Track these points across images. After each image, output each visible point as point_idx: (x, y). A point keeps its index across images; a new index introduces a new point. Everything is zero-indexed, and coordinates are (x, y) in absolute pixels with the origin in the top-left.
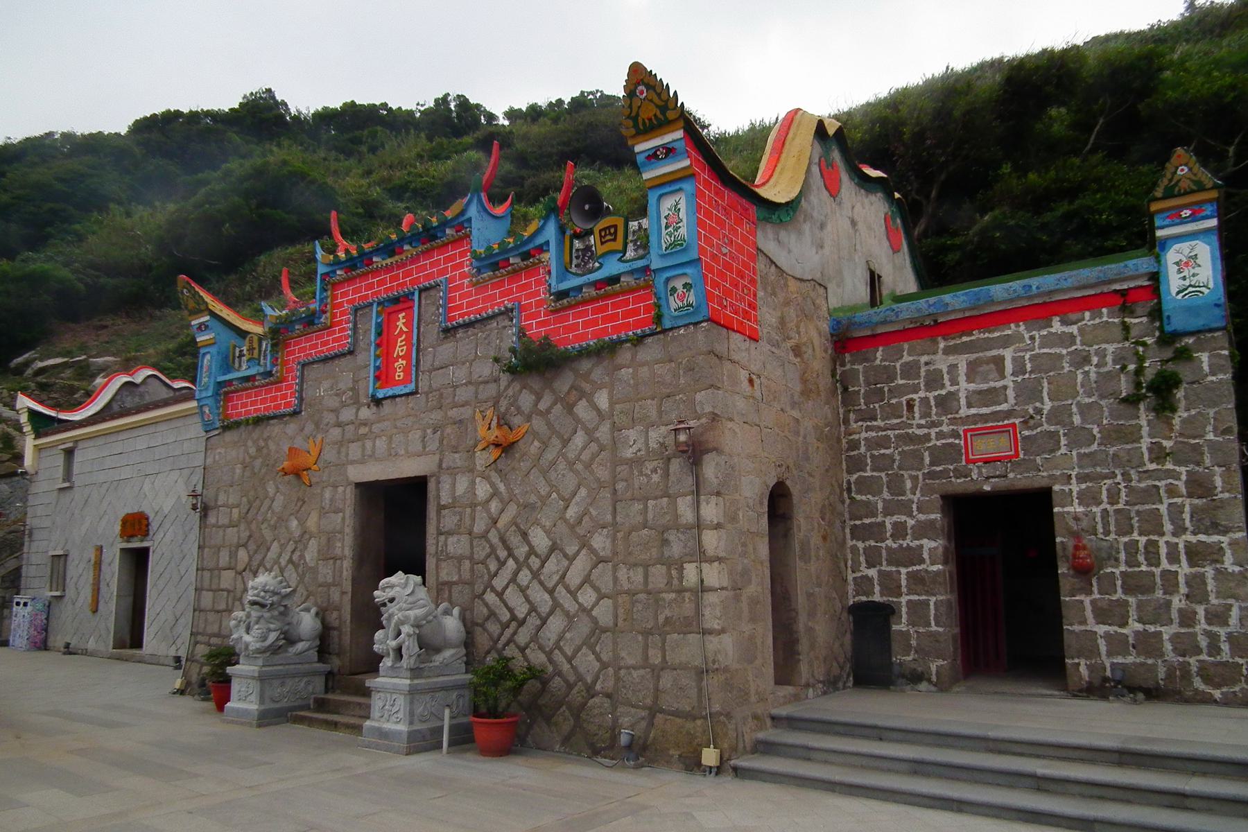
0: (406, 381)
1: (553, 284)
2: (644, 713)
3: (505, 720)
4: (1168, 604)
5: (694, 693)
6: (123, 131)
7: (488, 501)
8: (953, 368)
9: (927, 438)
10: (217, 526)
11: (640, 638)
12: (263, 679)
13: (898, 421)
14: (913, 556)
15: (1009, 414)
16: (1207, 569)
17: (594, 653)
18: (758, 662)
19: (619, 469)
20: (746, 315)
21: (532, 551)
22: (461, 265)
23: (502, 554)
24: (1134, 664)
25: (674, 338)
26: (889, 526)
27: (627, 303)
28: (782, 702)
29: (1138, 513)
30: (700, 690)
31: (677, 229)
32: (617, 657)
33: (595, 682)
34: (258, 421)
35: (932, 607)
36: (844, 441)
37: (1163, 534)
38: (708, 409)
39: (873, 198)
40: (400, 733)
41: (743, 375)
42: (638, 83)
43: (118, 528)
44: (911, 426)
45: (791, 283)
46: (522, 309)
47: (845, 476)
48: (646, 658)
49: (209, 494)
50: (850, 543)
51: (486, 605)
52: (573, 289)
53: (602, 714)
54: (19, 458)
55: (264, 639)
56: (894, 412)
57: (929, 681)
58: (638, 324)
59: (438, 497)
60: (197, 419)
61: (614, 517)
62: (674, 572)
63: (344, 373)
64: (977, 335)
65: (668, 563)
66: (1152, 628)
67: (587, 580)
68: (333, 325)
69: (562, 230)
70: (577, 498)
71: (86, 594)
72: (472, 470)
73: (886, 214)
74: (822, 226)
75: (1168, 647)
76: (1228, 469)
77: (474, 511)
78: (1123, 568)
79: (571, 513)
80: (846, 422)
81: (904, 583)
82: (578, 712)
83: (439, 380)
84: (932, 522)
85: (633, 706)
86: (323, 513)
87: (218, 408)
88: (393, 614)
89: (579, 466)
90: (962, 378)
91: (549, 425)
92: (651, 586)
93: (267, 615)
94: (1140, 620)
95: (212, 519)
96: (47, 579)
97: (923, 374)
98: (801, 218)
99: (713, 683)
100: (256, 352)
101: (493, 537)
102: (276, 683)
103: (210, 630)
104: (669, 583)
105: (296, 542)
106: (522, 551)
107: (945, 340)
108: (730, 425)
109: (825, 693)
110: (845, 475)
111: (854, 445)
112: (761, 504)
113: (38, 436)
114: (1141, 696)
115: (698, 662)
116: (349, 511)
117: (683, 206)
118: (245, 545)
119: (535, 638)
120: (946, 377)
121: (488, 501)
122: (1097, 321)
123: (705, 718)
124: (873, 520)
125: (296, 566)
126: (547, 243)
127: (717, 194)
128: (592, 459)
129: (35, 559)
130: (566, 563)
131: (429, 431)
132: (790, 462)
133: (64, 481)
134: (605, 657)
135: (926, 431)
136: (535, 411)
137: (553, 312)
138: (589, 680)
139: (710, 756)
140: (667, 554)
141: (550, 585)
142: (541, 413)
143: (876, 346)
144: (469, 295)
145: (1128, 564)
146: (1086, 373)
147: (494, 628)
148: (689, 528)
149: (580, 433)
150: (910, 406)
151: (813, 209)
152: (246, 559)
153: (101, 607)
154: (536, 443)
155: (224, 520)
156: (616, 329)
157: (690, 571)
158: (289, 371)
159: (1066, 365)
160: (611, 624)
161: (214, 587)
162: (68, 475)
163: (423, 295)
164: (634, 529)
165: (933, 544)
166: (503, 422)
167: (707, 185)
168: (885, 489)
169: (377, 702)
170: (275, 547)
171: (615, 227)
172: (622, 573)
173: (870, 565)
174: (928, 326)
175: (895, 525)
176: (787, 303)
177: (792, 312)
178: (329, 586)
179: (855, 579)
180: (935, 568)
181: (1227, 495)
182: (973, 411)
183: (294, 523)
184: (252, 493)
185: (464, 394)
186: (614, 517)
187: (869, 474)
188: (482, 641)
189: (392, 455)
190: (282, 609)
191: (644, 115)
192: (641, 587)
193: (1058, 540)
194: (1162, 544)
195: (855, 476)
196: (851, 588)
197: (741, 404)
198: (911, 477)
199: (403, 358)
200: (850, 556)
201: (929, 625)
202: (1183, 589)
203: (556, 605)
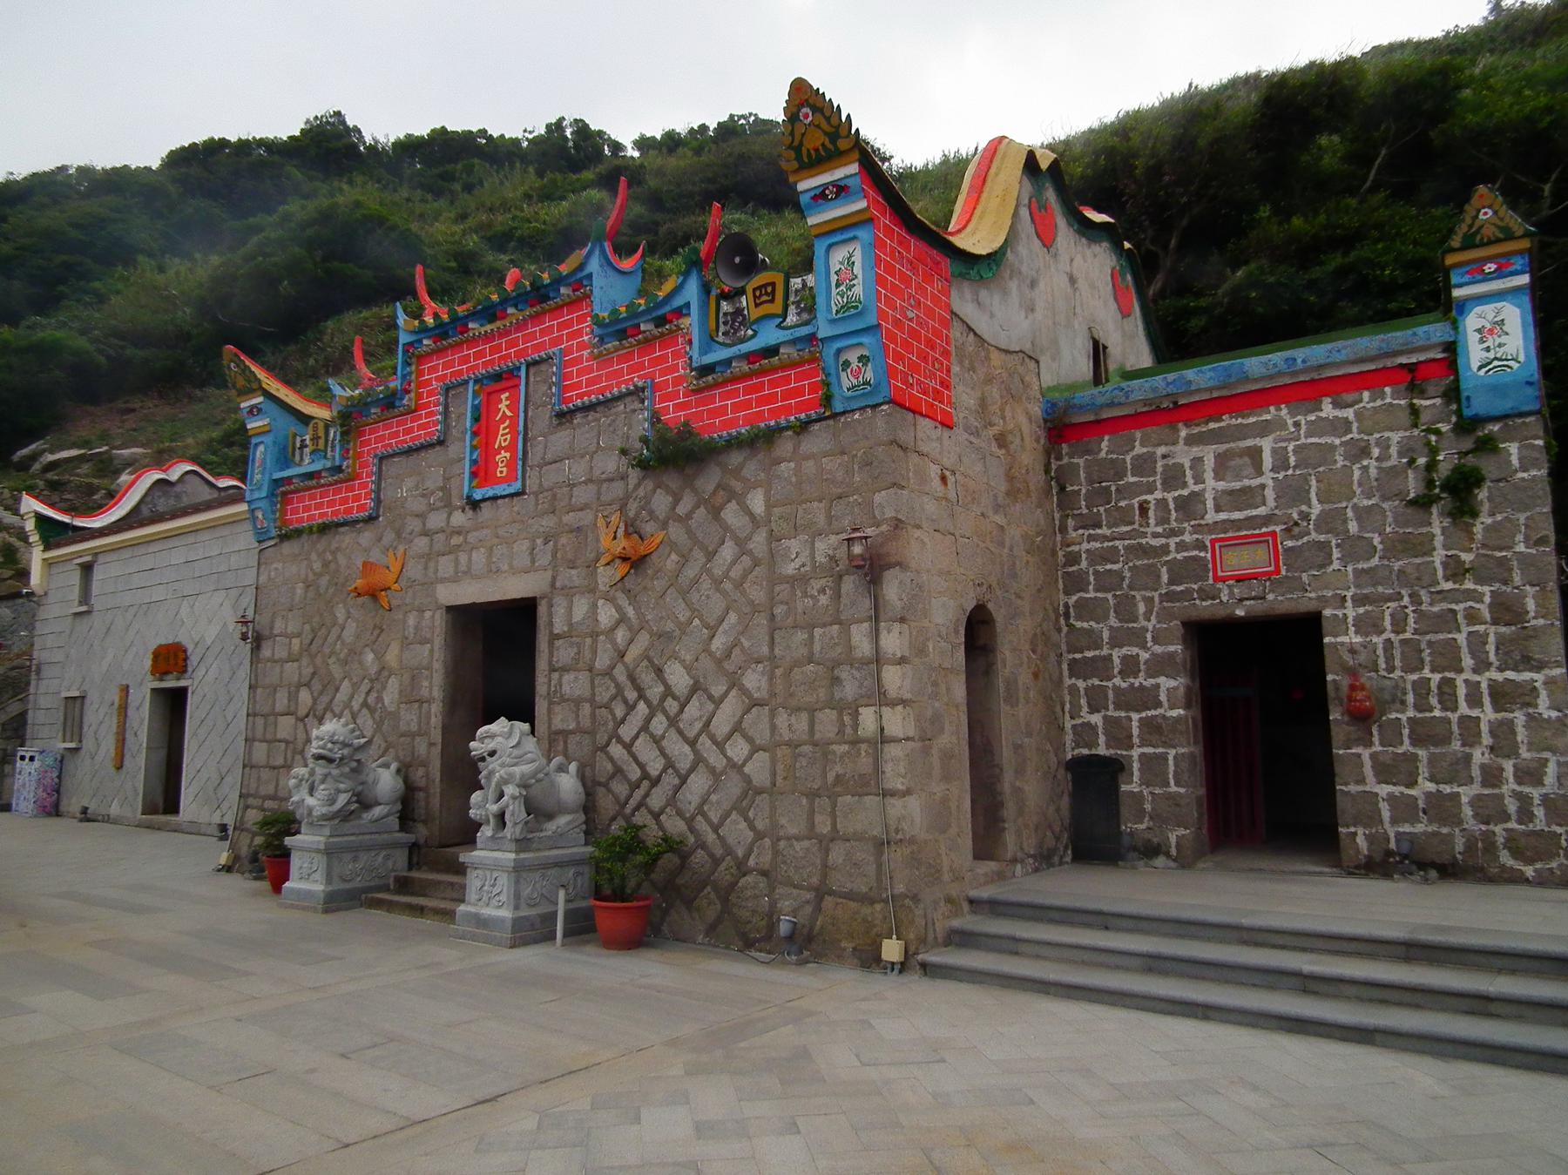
0: (509, 479)
1: (695, 356)
2: (809, 896)
3: (635, 903)
4: (1468, 759)
5: (871, 869)
6: (155, 164)
7: (613, 629)
8: (1197, 462)
9: (1165, 549)
12: (330, 852)
13: (1128, 528)
14: (1147, 699)
15: (1268, 519)
17: (746, 819)
18: (953, 830)
19: (777, 589)
20: (938, 395)
21: (668, 692)
22: (579, 333)
23: (631, 695)
24: (1425, 833)
26: (1117, 661)
27: (787, 380)
28: (982, 881)
29: (1430, 644)
30: (879, 866)
31: (850, 288)
32: (775, 826)
33: (747, 856)
34: (325, 529)
36: (1061, 553)
37: (1460, 671)
38: (889, 513)
39: (1097, 248)
41: (934, 471)
43: (148, 663)
44: (1144, 535)
45: (994, 355)
46: (656, 387)
48: (812, 825)
49: (263, 620)
51: (611, 759)
53: (756, 897)
54: (24, 574)
55: (332, 801)
56: (1124, 517)
57: (1168, 855)
58: (801, 407)
59: (551, 624)
60: (248, 526)
61: (772, 648)
62: (846, 719)
63: (432, 469)
64: (1227, 421)
66: (1447, 789)
67: (737, 728)
69: (706, 288)
70: (725, 625)
71: (108, 746)
73: (1113, 269)
74: (1033, 284)
75: (1468, 812)
76: (1543, 589)
78: (1411, 713)
79: (718, 644)
80: (1063, 529)
81: (1135, 731)
82: (727, 894)
83: (551, 476)
84: (1171, 655)
86: (406, 643)
87: (274, 512)
88: (494, 770)
90: (1209, 475)
92: (817, 736)
93: (335, 772)
94: (1432, 779)
95: (266, 652)
96: (59, 726)
97: (1159, 469)
99: (895, 857)
100: (322, 442)
101: (620, 674)
102: (347, 857)
103: (263, 792)
104: (841, 732)
105: (371, 681)
106: (655, 691)
107: (1187, 426)
109: (1036, 870)
110: (1062, 596)
111: (1073, 559)
113: (47, 548)
114: (1433, 874)
115: (876, 831)
116: (438, 642)
117: (858, 258)
119: (672, 801)
120: (1189, 473)
121: (613, 629)
122: (1379, 403)
123: (886, 901)
124: (1097, 653)
125: (372, 711)
126: (688, 305)
127: (900, 243)
128: (744, 577)
129: (44, 702)
130: (711, 707)
131: (539, 541)
132: (993, 580)
133: (81, 603)
134: (760, 825)
135: (1163, 541)
136: (672, 515)
138: (740, 853)
139: (892, 950)
140: (837, 696)
141: (691, 734)
142: (679, 519)
143: (1101, 434)
144: (589, 370)
145: (1417, 707)
147: (620, 788)
148: (865, 662)
150: (1143, 509)
151: (1021, 262)
152: (309, 702)
153: (127, 762)
154: (674, 557)
155: (281, 653)
157: (868, 717)
158: (364, 465)
160: (768, 783)
161: (269, 737)
162: (85, 597)
163: (532, 371)
164: (798, 663)
165: (1172, 683)
166: (632, 529)
167: (889, 232)
168: (1112, 613)
169: (473, 881)
170: (346, 687)
171: (773, 284)
172: (782, 719)
173: (1093, 709)
175: (1124, 658)
176: (989, 380)
177: (994, 392)
178: (413, 735)
179: (1074, 727)
180: (1175, 713)
181: (1541, 622)
182: (1223, 516)
183: (370, 657)
185: (583, 495)
186: (772, 648)
187: (1092, 595)
188: (606, 804)
189: (492, 571)
190: (354, 764)
192: (805, 737)
193: (1330, 677)
194: (1460, 682)
195: (1075, 598)
196: (1069, 738)
199: (506, 449)
200: (1067, 698)
202: (1487, 740)
203: (699, 760)
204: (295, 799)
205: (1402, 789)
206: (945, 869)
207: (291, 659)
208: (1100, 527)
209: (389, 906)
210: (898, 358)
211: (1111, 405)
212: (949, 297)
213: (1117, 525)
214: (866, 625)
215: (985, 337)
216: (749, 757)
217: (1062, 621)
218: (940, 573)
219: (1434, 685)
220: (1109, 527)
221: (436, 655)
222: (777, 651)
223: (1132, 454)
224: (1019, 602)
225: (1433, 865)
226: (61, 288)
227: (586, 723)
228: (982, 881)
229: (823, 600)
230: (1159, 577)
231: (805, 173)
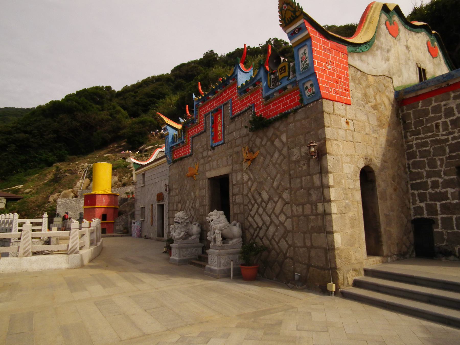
0: (221, 140)
1: (264, 94)
2: (305, 267)
3: (253, 267)
6: (169, 72)
9: (447, 140)
10: (173, 196)
11: (302, 235)
12: (179, 248)
13: (430, 134)
14: (443, 196)
17: (286, 241)
18: (357, 246)
20: (343, 94)
21: (263, 200)
23: (253, 202)
26: (429, 183)
27: (290, 97)
28: (374, 263)
30: (326, 258)
31: (305, 62)
34: (182, 159)
35: (454, 220)
36: (405, 145)
39: (419, 35)
41: (343, 120)
42: (283, 4)
43: (156, 198)
44: (438, 135)
45: (371, 79)
46: (255, 106)
47: (407, 161)
48: (305, 243)
50: (411, 191)
51: (249, 221)
55: (180, 234)
56: (430, 129)
57: (455, 255)
58: (295, 105)
59: (232, 181)
62: (314, 207)
67: (282, 211)
68: (200, 122)
70: (277, 179)
72: (242, 170)
74: (388, 51)
77: (243, 186)
79: (275, 184)
80: (406, 137)
81: (439, 209)
85: (301, 263)
86: (200, 189)
89: (277, 166)
91: (266, 150)
92: (305, 213)
93: (180, 226)
95: (171, 194)
101: (250, 195)
102: (184, 250)
104: (312, 212)
106: (259, 200)
107: (454, 92)
108: (335, 142)
109: (398, 260)
110: (407, 161)
112: (356, 176)
116: (207, 188)
117: (307, 52)
118: (180, 202)
119: (265, 235)
123: (328, 270)
124: (422, 180)
125: (194, 209)
126: (261, 78)
127: (324, 43)
130: (274, 205)
131: (228, 157)
134: (290, 242)
135: (446, 137)
137: (266, 105)
138: (284, 252)
141: (269, 214)
142: (263, 146)
143: (419, 100)
147: (252, 231)
148: (318, 188)
149: (277, 152)
150: (437, 126)
151: (382, 44)
153: (153, 224)
154: (262, 158)
156: (287, 108)
157: (320, 206)
160: (291, 229)
162: (144, 183)
163: (225, 107)
165: (453, 190)
166: (251, 151)
168: (427, 166)
169: (210, 258)
170: (188, 202)
171: (285, 66)
172: (294, 208)
173: (421, 201)
174: (445, 87)
175: (433, 182)
176: (368, 86)
179: (414, 208)
180: (455, 202)
183: (192, 194)
185: (238, 142)
187: (418, 159)
188: (248, 235)
189: (218, 167)
190: (185, 224)
191: (287, 17)
192: (301, 214)
195: (411, 161)
196: (412, 212)
197: (342, 133)
198: (439, 159)
199: (221, 131)
201: (453, 229)
203: (272, 222)
207: (177, 195)
208: (420, 134)
212: (347, 59)
214: (318, 175)
215: (365, 72)
216: (286, 221)
217: (407, 170)
218: (347, 155)
220: (424, 134)
222: (292, 186)
223: (431, 106)
226: (149, 107)
228: (374, 263)
229: (305, 168)
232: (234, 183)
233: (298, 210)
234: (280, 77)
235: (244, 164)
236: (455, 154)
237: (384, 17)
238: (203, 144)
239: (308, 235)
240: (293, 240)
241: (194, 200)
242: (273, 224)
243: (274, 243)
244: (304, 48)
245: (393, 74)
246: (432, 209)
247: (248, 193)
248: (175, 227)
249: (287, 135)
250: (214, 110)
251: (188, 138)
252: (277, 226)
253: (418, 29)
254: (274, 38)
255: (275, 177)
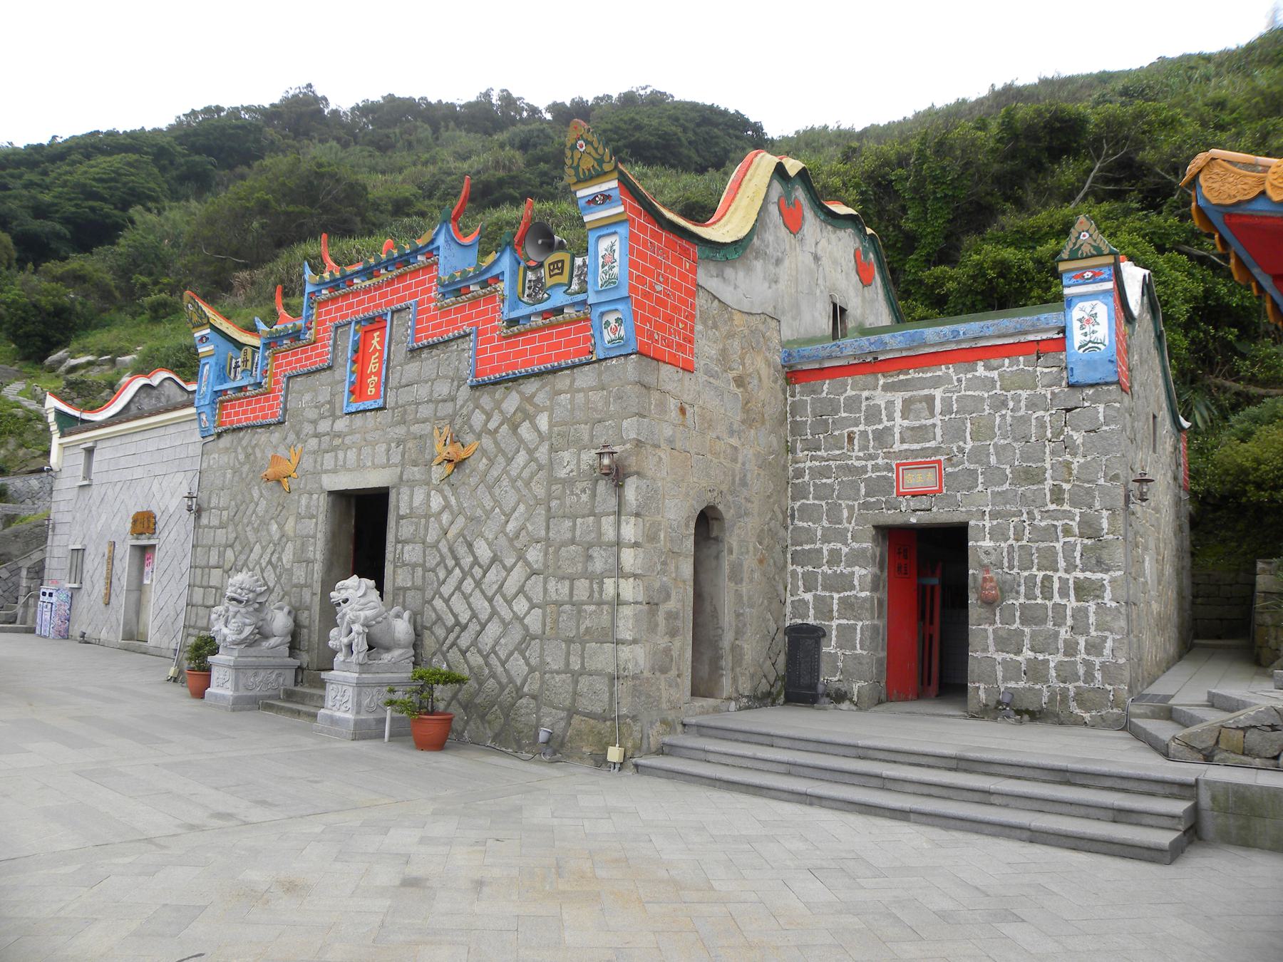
0: (377, 395)
1: (506, 312)
2: (564, 714)
4: (1057, 634)
5: (606, 697)
7: (440, 513)
8: (890, 404)
9: (864, 470)
12: (237, 668)
13: (838, 452)
14: (843, 583)
15: (937, 450)
16: (1091, 603)
18: (674, 672)
19: (554, 488)
21: (476, 562)
22: (430, 290)
23: (451, 563)
24: (1024, 688)
25: (607, 368)
27: (568, 332)
29: (1037, 549)
30: (612, 694)
31: (611, 268)
32: (543, 663)
33: (523, 685)
36: (791, 469)
37: (1057, 570)
38: (633, 435)
39: (841, 234)
40: (347, 720)
41: (673, 404)
43: (129, 525)
44: (850, 458)
45: (737, 316)
48: (568, 664)
49: (204, 496)
51: (434, 610)
52: (522, 317)
53: (528, 714)
54: (47, 453)
55: (241, 632)
57: (851, 700)
59: (398, 507)
60: (196, 425)
61: (547, 533)
63: (322, 388)
64: (913, 374)
65: (590, 577)
66: (1040, 657)
67: (521, 590)
70: (516, 514)
71: (100, 587)
72: (428, 483)
73: (856, 251)
74: (778, 262)
75: (1053, 673)
76: (1114, 512)
78: (1022, 600)
79: (511, 527)
80: (791, 450)
81: (835, 607)
82: (508, 710)
83: (405, 396)
84: (864, 550)
86: (299, 517)
87: (214, 416)
88: (347, 612)
90: (898, 415)
91: (496, 443)
93: (243, 610)
94: (1032, 649)
95: (204, 521)
96: (67, 570)
97: (863, 408)
98: (751, 257)
99: (622, 688)
100: (249, 364)
102: (251, 673)
103: (200, 624)
104: (591, 596)
105: (275, 545)
106: (467, 561)
109: (749, 708)
111: (799, 474)
113: (63, 436)
114: (1026, 717)
115: (611, 669)
116: (321, 517)
117: (617, 247)
118: (231, 546)
119: (474, 643)
120: (884, 412)
121: (440, 513)
122: (1015, 368)
125: (274, 568)
128: (531, 478)
129: (57, 552)
130: (504, 574)
131: (393, 445)
132: (724, 488)
133: (84, 478)
134: (533, 662)
135: (864, 463)
137: (505, 338)
139: (614, 754)
140: (590, 569)
141: (490, 594)
142: (489, 432)
144: (435, 317)
145: (1027, 597)
146: (1003, 417)
147: (440, 632)
150: (851, 438)
151: (767, 246)
152: (233, 559)
153: (112, 600)
154: (484, 460)
155: (215, 522)
157: (609, 584)
158: (277, 382)
159: (986, 407)
161: (205, 584)
162: (87, 473)
163: (396, 316)
164: (564, 544)
165: (864, 572)
167: (642, 229)
169: (331, 692)
170: (257, 548)
171: (563, 261)
172: (552, 584)
175: (831, 551)
176: (731, 335)
177: (736, 344)
178: (302, 586)
180: (863, 594)
181: (1111, 536)
182: (905, 446)
183: (274, 527)
184: (240, 497)
185: (425, 411)
186: (547, 533)
187: (811, 502)
188: (429, 642)
189: (360, 467)
192: (567, 599)
193: (971, 572)
194: (1055, 579)
196: (788, 609)
198: (848, 506)
200: (790, 580)
201: (855, 648)
202: (1069, 622)
203: (494, 612)
204: (215, 628)
205: (1012, 656)
206: (664, 700)
209: (280, 709)
210: (645, 320)
211: (830, 357)
212: (695, 274)
213: (831, 449)
216: (528, 613)
219: (1038, 580)
221: (320, 527)
224: (749, 505)
225: (1027, 712)
227: (419, 582)
229: (584, 497)
230: (859, 490)
231: (581, 185)
232: (401, 513)
233: (558, 589)
234: (549, 282)
235: (434, 468)
236: (873, 500)
237: (777, 188)
238: (321, 399)
239: (576, 647)
240: (541, 656)
241: (279, 545)
242: (495, 619)
243: (493, 660)
244: (613, 239)
245: (783, 313)
246: (824, 609)
247: (438, 542)
248: (227, 611)
249: (550, 417)
250: (366, 320)
251: (275, 375)
252: (505, 624)
253: (840, 222)
254: (503, 91)
255: (514, 510)
